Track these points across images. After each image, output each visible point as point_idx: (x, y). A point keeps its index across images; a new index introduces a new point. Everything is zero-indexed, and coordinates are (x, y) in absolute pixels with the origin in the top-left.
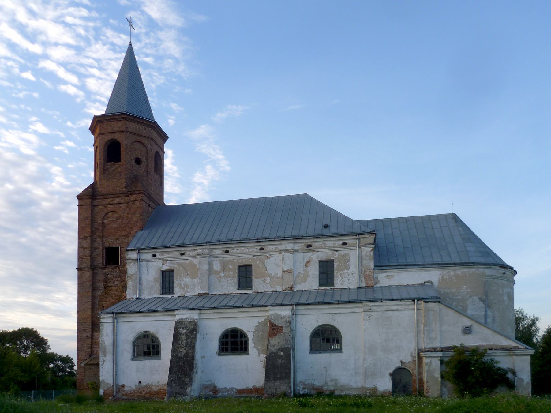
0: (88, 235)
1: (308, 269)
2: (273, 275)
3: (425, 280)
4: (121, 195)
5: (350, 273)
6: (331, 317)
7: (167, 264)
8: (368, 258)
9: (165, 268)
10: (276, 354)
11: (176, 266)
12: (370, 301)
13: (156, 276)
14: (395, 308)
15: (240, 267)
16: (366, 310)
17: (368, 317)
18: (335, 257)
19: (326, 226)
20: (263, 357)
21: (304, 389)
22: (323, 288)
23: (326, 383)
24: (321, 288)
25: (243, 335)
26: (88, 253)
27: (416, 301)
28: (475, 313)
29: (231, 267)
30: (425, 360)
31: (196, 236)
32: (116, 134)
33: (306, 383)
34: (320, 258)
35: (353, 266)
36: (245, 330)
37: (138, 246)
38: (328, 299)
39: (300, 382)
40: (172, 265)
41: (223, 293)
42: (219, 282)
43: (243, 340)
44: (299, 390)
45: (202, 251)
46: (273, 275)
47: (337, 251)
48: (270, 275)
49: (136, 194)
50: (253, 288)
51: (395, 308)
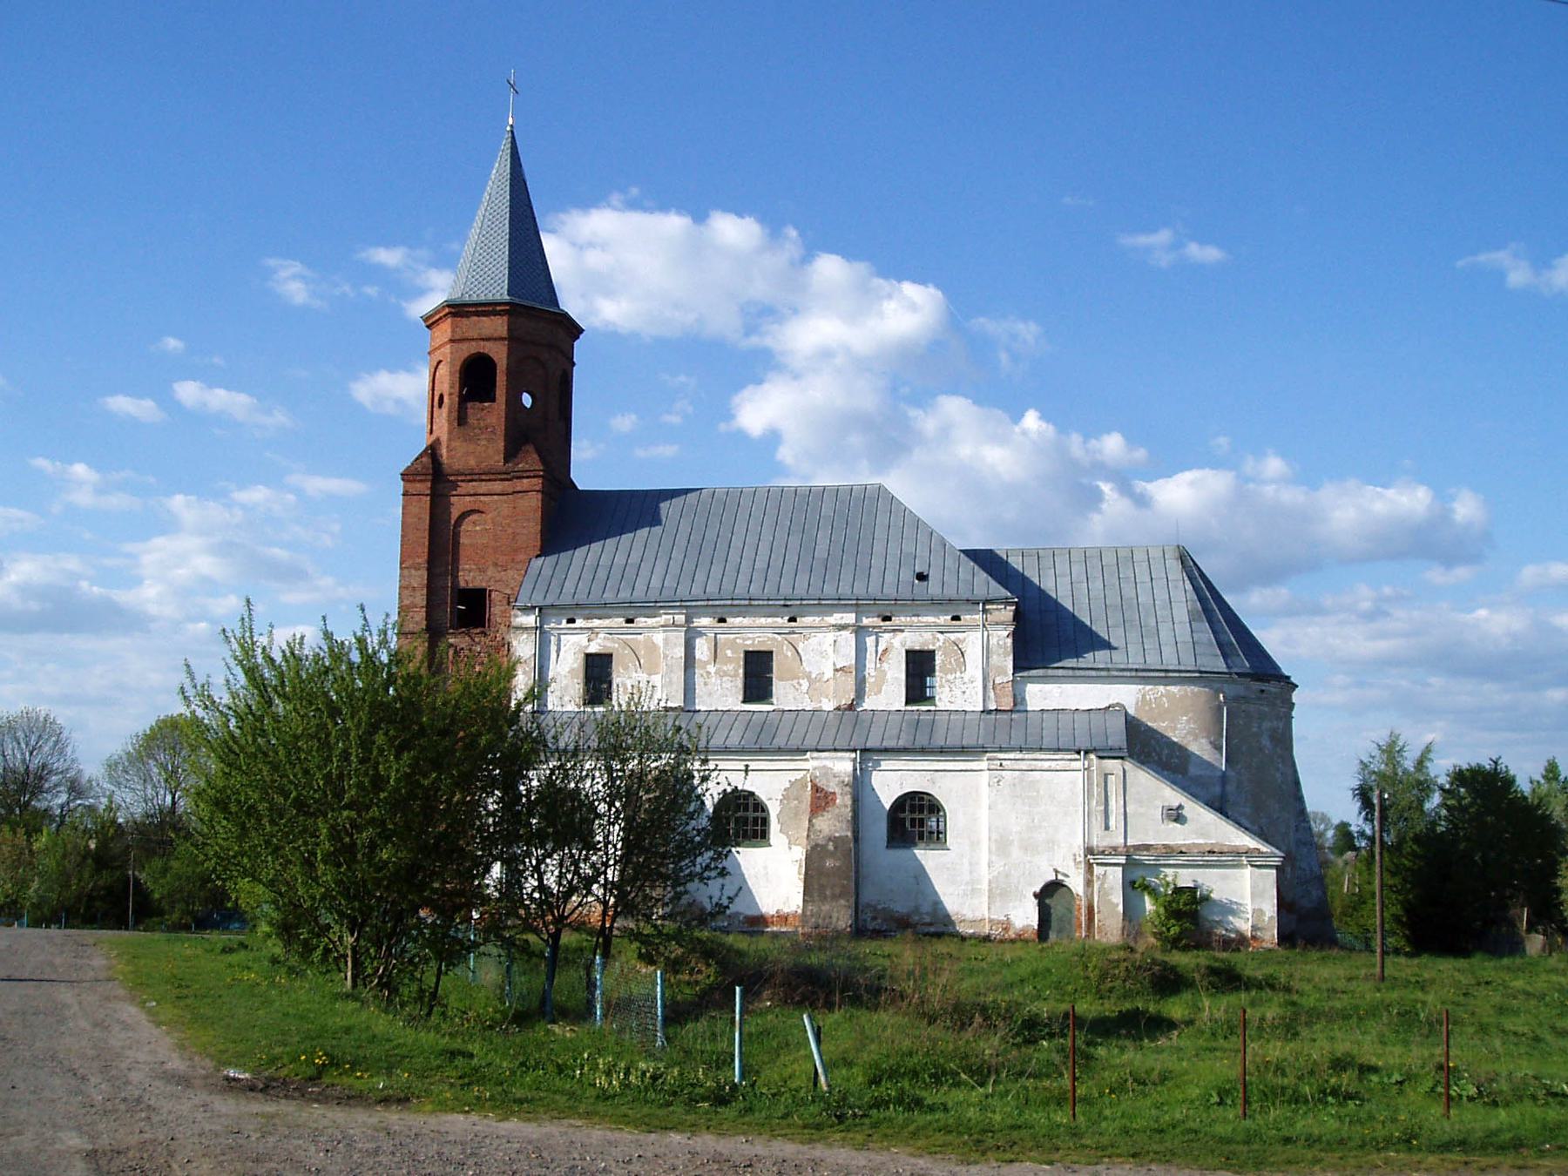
0: (422, 559)
1: (885, 666)
2: (813, 676)
3: (1111, 702)
4: (492, 477)
5: (966, 680)
6: (929, 778)
7: (599, 641)
8: (1001, 651)
9: (594, 648)
10: (824, 847)
11: (617, 645)
12: (1001, 750)
13: (575, 665)
14: (1046, 765)
15: (747, 653)
16: (992, 767)
17: (996, 780)
18: (937, 645)
19: (922, 577)
20: (799, 853)
21: (874, 918)
22: (915, 708)
23: (917, 909)
24: (909, 708)
25: (760, 807)
26: (420, 598)
27: (1082, 753)
28: (1202, 773)
29: (729, 653)
30: (1098, 870)
31: (656, 583)
32: (487, 344)
33: (880, 907)
34: (909, 646)
35: (974, 669)
36: (762, 795)
37: (538, 599)
38: (922, 741)
39: (868, 905)
40: (609, 644)
41: (713, 709)
42: (706, 684)
43: (759, 814)
44: (865, 920)
45: (671, 617)
46: (813, 676)
47: (942, 632)
48: (808, 676)
49: (528, 477)
50: (774, 700)
51: (1046, 765)
